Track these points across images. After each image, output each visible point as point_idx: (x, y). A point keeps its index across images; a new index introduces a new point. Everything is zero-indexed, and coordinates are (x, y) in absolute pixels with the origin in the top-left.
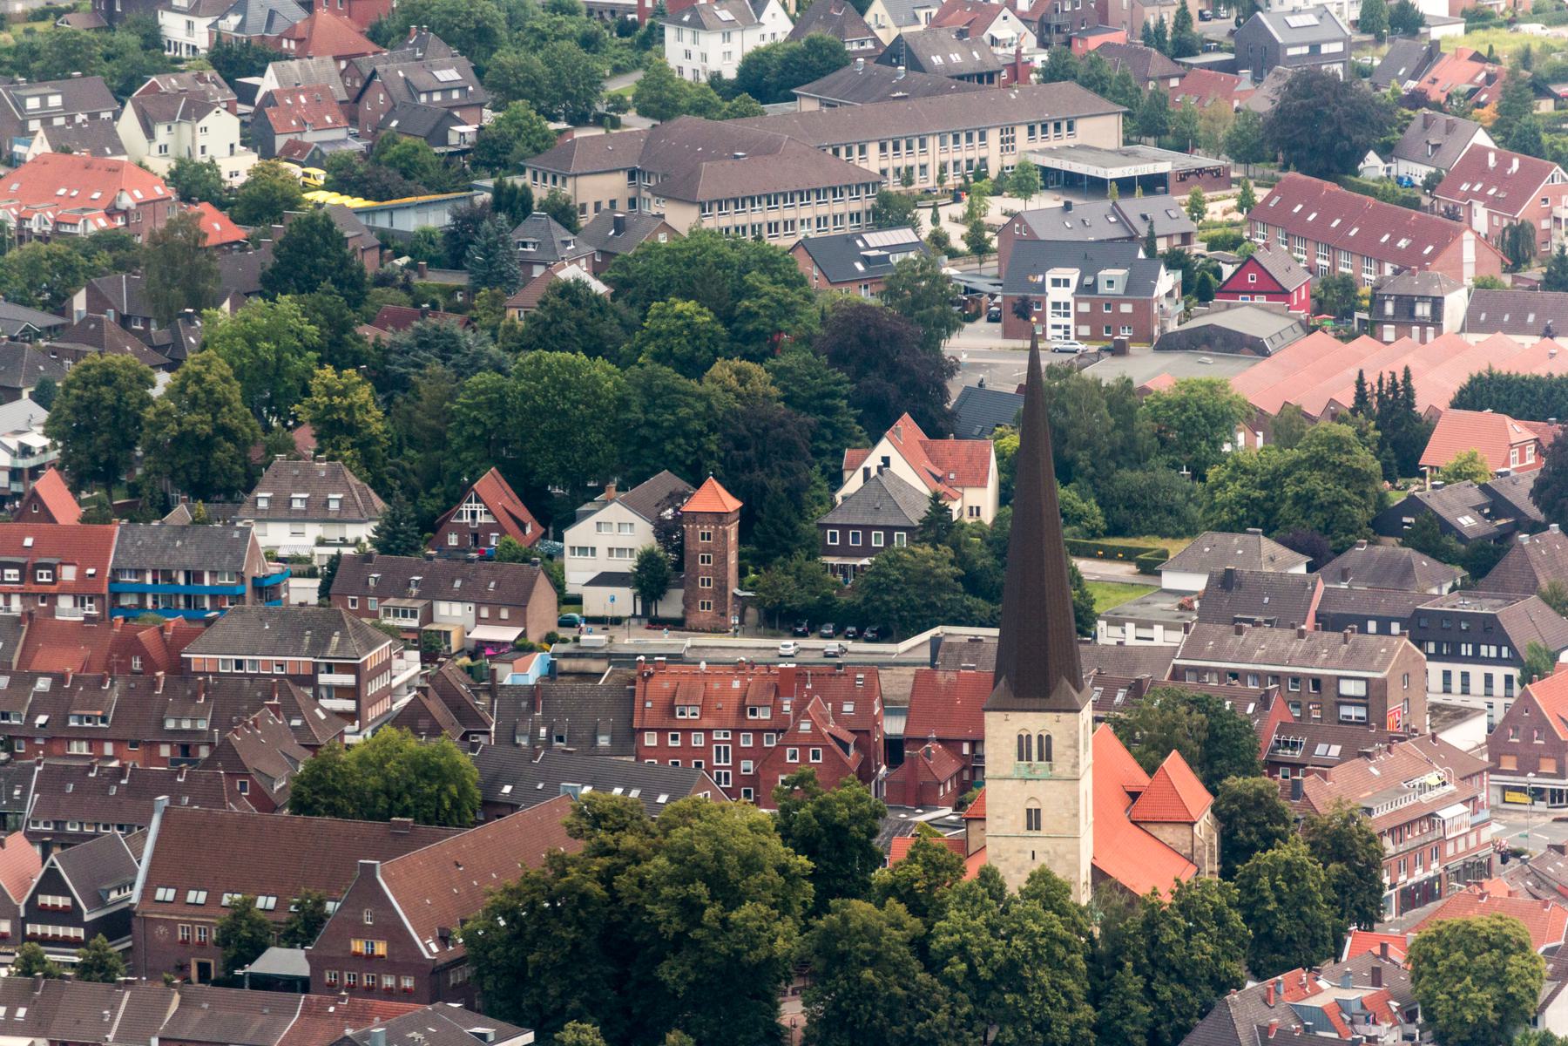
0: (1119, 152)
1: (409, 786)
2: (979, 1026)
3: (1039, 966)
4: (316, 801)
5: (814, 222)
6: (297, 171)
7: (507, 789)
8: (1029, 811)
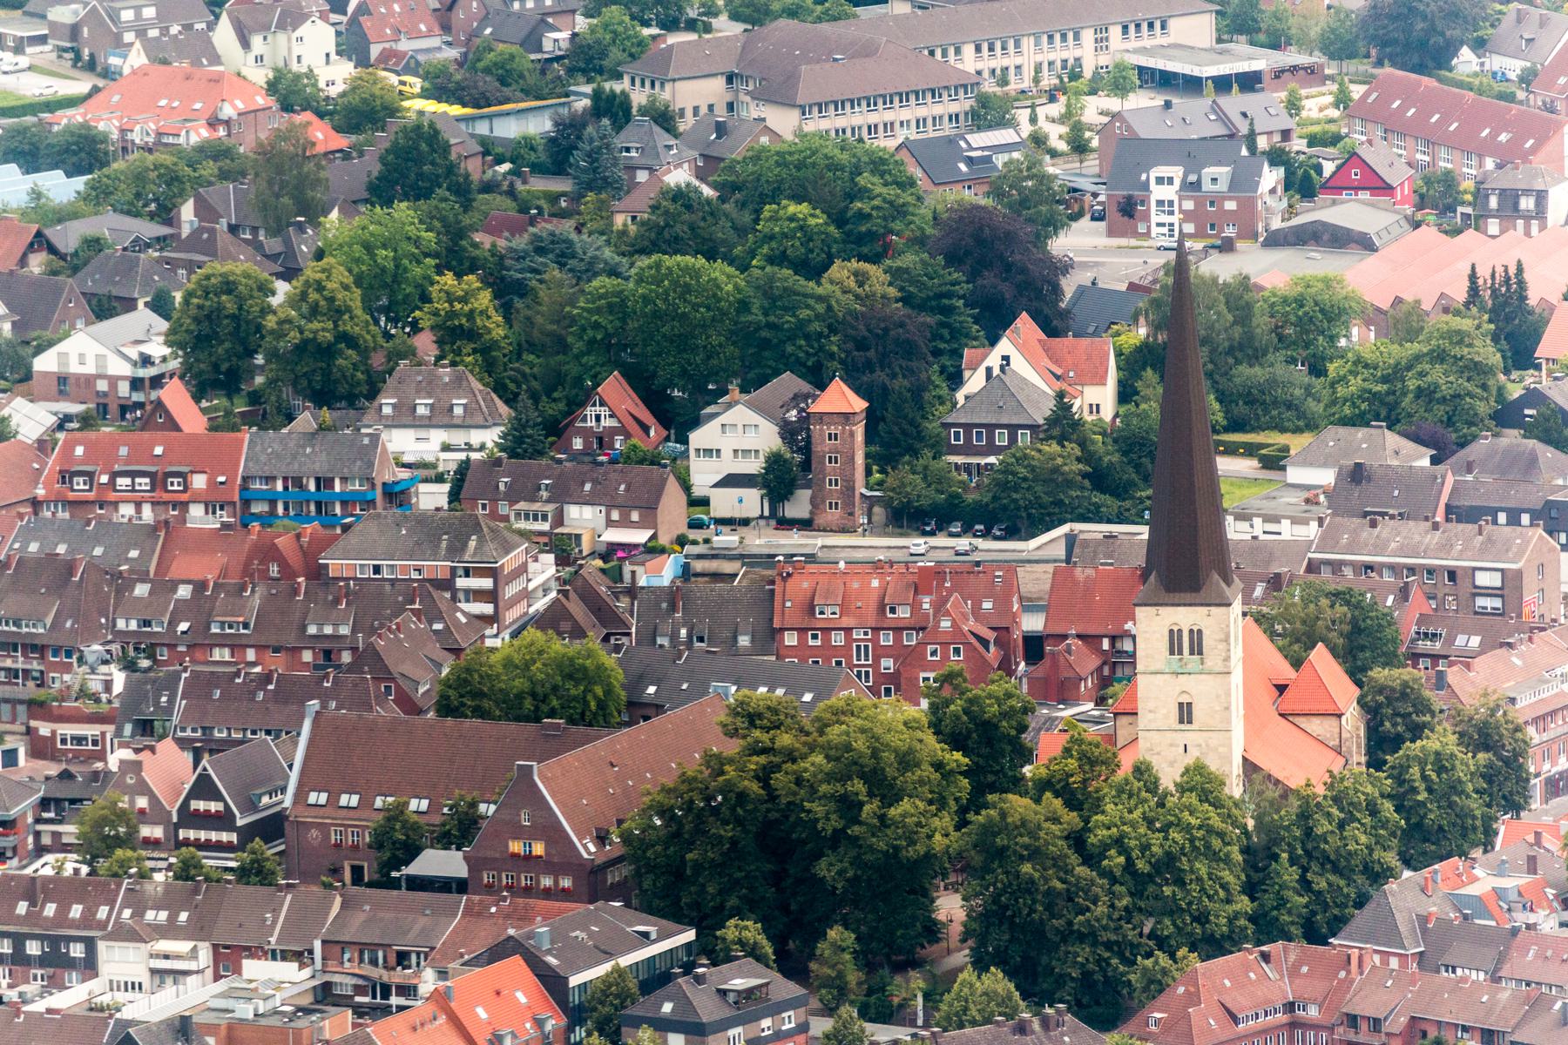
0: (1211, 50)
1: (555, 688)
2: (1137, 918)
3: (1196, 858)
4: (463, 705)
5: (913, 124)
6: (394, 79)
7: (652, 690)
8: (1181, 704)
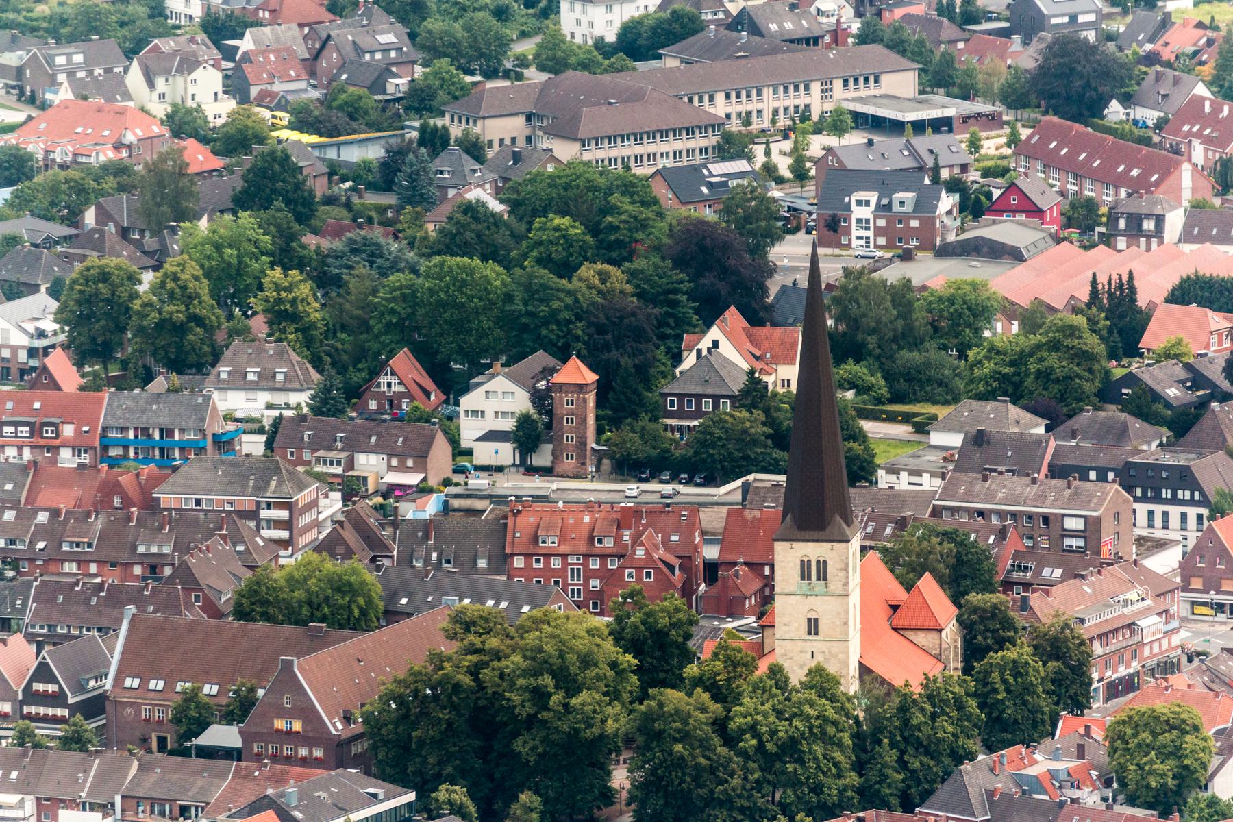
0: (914, 100)
3: (814, 742)
4: (253, 610)
5: (671, 155)
6: (266, 114)
7: (404, 601)
8: (809, 620)
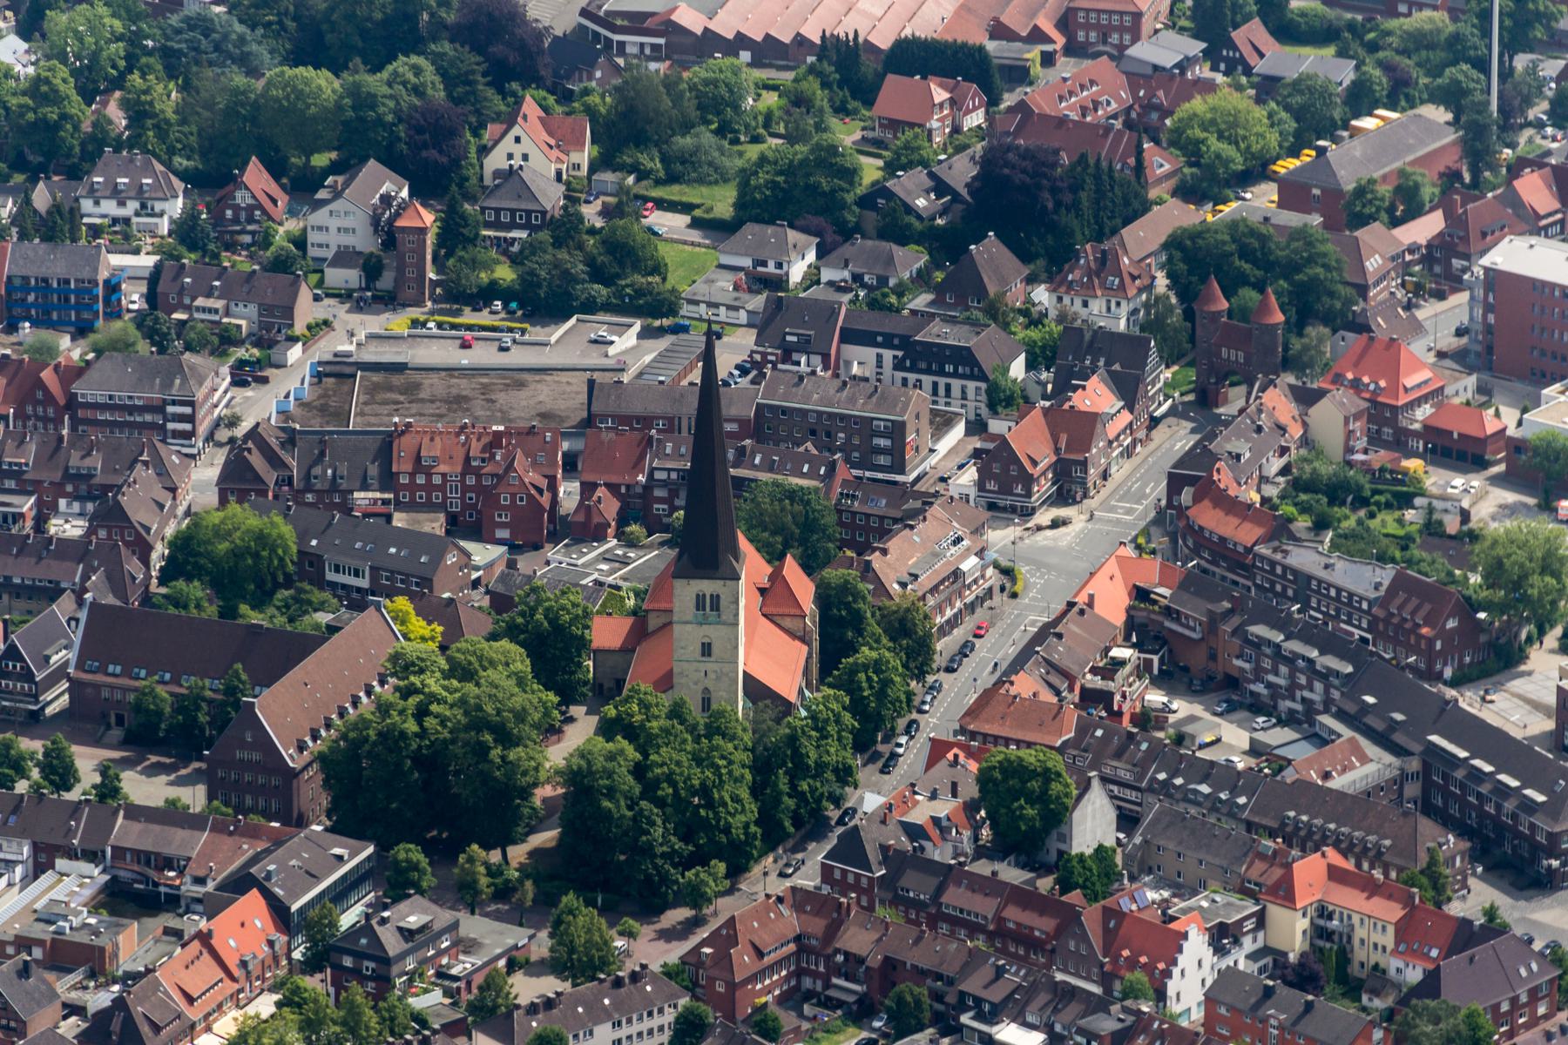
7: (314, 543)
